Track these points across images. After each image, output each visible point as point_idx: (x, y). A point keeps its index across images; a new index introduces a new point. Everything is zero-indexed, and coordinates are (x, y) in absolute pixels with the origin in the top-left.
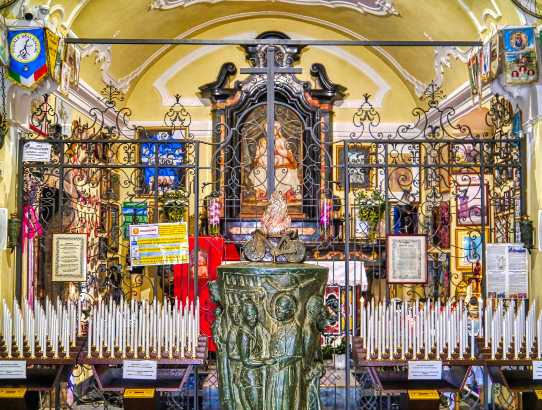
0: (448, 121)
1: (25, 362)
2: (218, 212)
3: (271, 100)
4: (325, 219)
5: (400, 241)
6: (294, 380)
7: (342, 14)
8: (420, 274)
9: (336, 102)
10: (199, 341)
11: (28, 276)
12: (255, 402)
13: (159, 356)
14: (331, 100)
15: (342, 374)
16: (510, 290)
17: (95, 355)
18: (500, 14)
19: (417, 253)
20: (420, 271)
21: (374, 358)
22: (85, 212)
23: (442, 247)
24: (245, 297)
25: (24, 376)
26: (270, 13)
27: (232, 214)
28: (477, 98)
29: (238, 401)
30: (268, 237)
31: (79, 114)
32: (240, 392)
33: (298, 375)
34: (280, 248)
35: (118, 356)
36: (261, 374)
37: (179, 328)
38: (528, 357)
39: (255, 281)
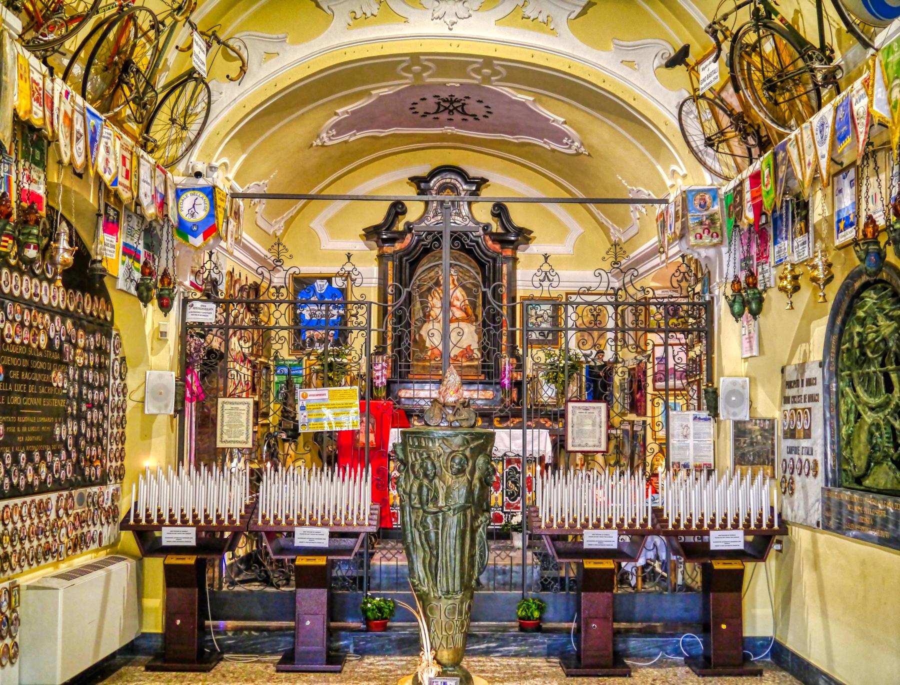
0: (631, 281)
1: (195, 529)
2: (385, 372)
3: (446, 242)
4: (506, 382)
5: (579, 408)
7: (526, 148)
8: (600, 442)
9: (521, 247)
10: (371, 509)
12: (433, 542)
13: (331, 523)
14: (514, 245)
15: (520, 552)
16: (695, 460)
18: (685, 172)
19: (598, 420)
20: (600, 439)
21: (549, 527)
22: (241, 372)
23: (638, 415)
24: (425, 455)
25: (193, 543)
26: (445, 144)
27: (401, 374)
28: (664, 257)
29: (418, 543)
30: (444, 405)
31: (232, 264)
32: (420, 535)
33: (469, 521)
34: (455, 415)
35: (290, 523)
36: (438, 520)
37: (349, 496)
38: (706, 527)
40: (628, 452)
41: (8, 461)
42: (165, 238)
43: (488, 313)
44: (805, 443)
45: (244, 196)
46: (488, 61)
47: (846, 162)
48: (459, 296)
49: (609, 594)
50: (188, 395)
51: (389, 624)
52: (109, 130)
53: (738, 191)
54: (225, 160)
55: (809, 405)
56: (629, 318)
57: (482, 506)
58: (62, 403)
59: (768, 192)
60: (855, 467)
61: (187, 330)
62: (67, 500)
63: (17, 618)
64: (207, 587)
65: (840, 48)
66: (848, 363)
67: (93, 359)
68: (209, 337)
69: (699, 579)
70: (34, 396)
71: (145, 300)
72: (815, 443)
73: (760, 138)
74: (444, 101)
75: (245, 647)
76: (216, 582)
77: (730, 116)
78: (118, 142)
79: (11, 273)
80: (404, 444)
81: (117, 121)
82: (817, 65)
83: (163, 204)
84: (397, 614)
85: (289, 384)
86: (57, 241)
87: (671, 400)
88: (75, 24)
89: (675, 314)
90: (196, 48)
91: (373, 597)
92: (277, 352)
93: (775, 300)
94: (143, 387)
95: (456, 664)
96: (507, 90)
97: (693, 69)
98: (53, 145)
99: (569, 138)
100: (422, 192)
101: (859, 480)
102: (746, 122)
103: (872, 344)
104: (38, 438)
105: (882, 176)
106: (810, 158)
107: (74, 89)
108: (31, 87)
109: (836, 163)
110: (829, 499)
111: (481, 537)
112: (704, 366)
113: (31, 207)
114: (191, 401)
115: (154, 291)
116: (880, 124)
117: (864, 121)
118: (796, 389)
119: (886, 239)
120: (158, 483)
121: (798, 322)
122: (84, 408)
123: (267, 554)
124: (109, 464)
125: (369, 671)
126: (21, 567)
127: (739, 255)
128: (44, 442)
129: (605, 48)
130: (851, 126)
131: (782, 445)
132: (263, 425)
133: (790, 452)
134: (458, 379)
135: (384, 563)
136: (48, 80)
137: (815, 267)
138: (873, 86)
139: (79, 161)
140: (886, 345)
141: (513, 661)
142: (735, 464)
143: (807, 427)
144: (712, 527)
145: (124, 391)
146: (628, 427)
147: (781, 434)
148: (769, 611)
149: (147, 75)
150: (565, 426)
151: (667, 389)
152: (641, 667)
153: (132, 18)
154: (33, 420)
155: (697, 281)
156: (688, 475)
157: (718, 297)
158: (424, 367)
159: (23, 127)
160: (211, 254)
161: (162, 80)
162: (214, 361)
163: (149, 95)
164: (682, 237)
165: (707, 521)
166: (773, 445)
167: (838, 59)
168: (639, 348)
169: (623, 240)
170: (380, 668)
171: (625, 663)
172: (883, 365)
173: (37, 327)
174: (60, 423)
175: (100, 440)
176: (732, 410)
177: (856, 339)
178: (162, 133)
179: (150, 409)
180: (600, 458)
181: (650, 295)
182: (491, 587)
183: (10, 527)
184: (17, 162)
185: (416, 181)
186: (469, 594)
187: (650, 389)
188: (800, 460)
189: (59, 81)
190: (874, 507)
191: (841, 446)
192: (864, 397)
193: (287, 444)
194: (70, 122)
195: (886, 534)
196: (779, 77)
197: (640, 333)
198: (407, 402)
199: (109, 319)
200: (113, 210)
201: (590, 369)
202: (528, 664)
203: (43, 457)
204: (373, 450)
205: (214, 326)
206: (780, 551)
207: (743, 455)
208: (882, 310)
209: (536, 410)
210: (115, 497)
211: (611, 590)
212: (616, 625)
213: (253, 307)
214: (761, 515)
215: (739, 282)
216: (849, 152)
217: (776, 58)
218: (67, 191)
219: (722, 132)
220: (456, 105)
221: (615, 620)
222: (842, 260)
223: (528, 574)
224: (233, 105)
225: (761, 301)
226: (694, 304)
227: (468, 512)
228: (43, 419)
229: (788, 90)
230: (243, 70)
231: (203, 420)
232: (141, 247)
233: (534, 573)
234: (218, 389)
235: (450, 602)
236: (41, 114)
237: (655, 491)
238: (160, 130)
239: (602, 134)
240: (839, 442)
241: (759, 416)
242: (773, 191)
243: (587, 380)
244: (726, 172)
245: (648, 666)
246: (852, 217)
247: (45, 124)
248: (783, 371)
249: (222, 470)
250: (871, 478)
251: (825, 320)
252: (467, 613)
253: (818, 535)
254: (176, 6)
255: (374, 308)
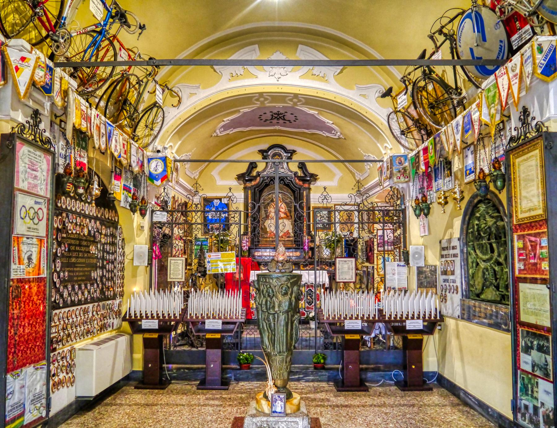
3: (277, 181)
4: (306, 247)
6: (288, 319)
7: (314, 136)
9: (312, 183)
11: (155, 280)
14: (309, 182)
15: (314, 331)
17: (191, 317)
18: (391, 147)
19: (351, 267)
21: (328, 319)
23: (370, 263)
24: (268, 286)
25: (157, 327)
26: (275, 134)
27: (255, 244)
28: (382, 187)
29: (266, 328)
30: (278, 262)
35: (203, 318)
37: (230, 304)
38: (404, 318)
39: (272, 279)
40: (366, 281)
41: (70, 289)
42: (143, 181)
43: (297, 215)
44: (451, 277)
45: (180, 161)
46: (296, 95)
47: (469, 142)
48: (283, 207)
49: (357, 351)
50: (154, 256)
51: (251, 366)
52: (117, 132)
53: (417, 156)
54: (171, 144)
55: (453, 259)
56: (365, 217)
57: (296, 310)
58: (95, 261)
59: (432, 157)
60: (476, 289)
61: (153, 225)
62: (97, 307)
63: (74, 364)
64: (164, 349)
65: (465, 88)
66: (472, 239)
67: (109, 240)
68: (164, 228)
69: (401, 343)
70: (81, 258)
71: (134, 211)
72: (456, 277)
73: (427, 131)
74: (275, 114)
75: (182, 377)
76: (168, 345)
77: (413, 120)
78: (121, 137)
79: (71, 200)
80: (258, 280)
81: (121, 127)
82: (454, 97)
83: (142, 166)
84: (255, 361)
85: (201, 250)
86: (93, 184)
87: (386, 256)
88: (102, 83)
89: (387, 214)
90: (157, 92)
91: (243, 353)
92: (196, 235)
93: (436, 209)
94: (132, 253)
95: (284, 387)
96: (305, 109)
97: (394, 98)
98: (91, 140)
99: (335, 131)
100: (265, 158)
101: (478, 295)
102: (420, 123)
103: (484, 230)
104: (84, 278)
105: (487, 149)
106: (452, 140)
107: (101, 113)
108: (81, 113)
109: (464, 143)
110: (464, 305)
111: (296, 325)
112: (402, 240)
113: (81, 169)
114: (155, 259)
115: (138, 207)
116: (485, 125)
117: (478, 123)
118: (447, 251)
119: (489, 179)
120: (140, 299)
121: (447, 219)
122: (105, 263)
123: (192, 332)
124: (117, 290)
125: (242, 389)
126: (76, 339)
127: (418, 187)
128: (86, 280)
129: (351, 89)
130: (471, 125)
131: (440, 278)
132: (189, 269)
133: (444, 282)
134: (284, 249)
135: (248, 336)
136: (89, 110)
137: (455, 193)
138: (481, 107)
139: (103, 147)
140: (490, 230)
141: (311, 384)
142: (418, 288)
143: (452, 269)
144: (407, 318)
145: (124, 255)
146: (365, 269)
147: (440, 273)
148: (435, 359)
149: (135, 105)
150: (335, 269)
151: (384, 251)
152: (373, 387)
153: (128, 79)
154: (81, 269)
155: (398, 199)
156: (395, 293)
157: (408, 207)
158: (266, 241)
159: (77, 132)
160: (164, 189)
161: (141, 108)
162: (166, 239)
163: (136, 115)
164: (390, 178)
165: (404, 316)
166: (436, 278)
167: (464, 93)
168: (370, 232)
169: (362, 179)
170: (247, 387)
171: (365, 385)
172: (489, 239)
173: (83, 225)
174: (94, 271)
175: (112, 278)
176: (416, 261)
177: (476, 227)
178: (141, 132)
179: (136, 263)
180: (352, 285)
181: (376, 205)
182: (300, 347)
183: (71, 320)
184: (74, 148)
185: (262, 152)
186: (290, 353)
187: (376, 252)
188: (449, 286)
189: (94, 109)
190: (486, 309)
191: (469, 279)
192: (480, 255)
193: (201, 279)
194: (99, 128)
195: (492, 322)
196: (436, 102)
197: (371, 224)
198: (258, 258)
199: (116, 220)
200: (119, 169)
201: (346, 241)
202: (319, 385)
203: (86, 287)
204: (242, 281)
205: (166, 223)
206: (440, 330)
207: (422, 283)
208: (488, 213)
209: (321, 261)
210: (120, 305)
211: (358, 349)
212: (361, 366)
213: (184, 214)
214: (431, 312)
215: (418, 200)
216: (471, 137)
217: (434, 93)
218: (97, 161)
219: (409, 128)
220: (280, 116)
221: (360, 364)
222: (468, 189)
223: (318, 341)
224: (175, 119)
225: (429, 209)
226: (396, 210)
227: (290, 314)
228: (86, 269)
229: (440, 108)
230: (179, 102)
231: (161, 268)
232: (132, 186)
233: (321, 341)
234: (168, 253)
235: (281, 357)
236: (85, 125)
237: (379, 301)
238: (141, 131)
239: (351, 129)
240: (468, 277)
241: (429, 264)
242: (434, 156)
243: (345, 247)
244: (411, 147)
245: (377, 386)
246: (472, 169)
247: (87, 130)
248: (440, 242)
249: (170, 292)
250: (484, 295)
251: (461, 218)
252: (289, 362)
253: (459, 322)
254: (148, 73)
255: (242, 213)
